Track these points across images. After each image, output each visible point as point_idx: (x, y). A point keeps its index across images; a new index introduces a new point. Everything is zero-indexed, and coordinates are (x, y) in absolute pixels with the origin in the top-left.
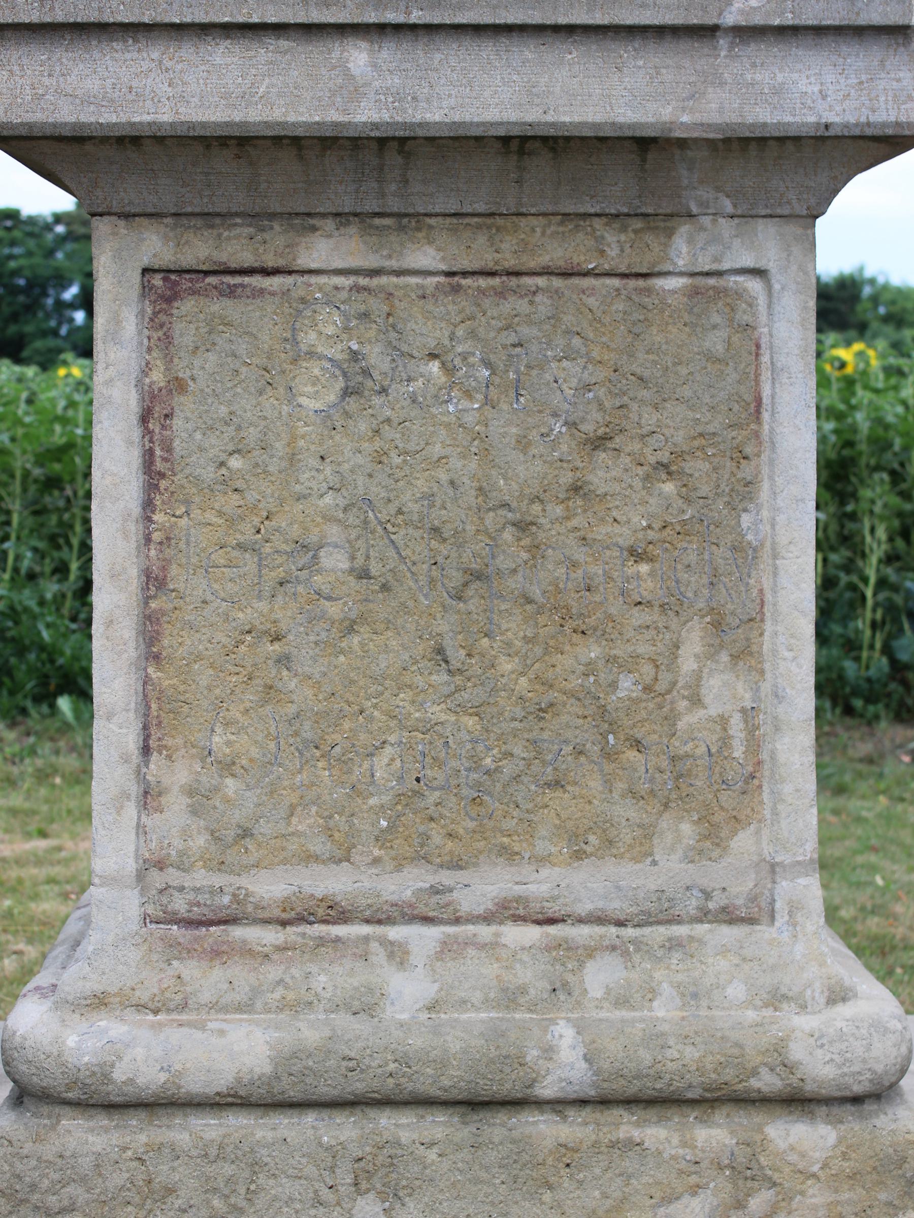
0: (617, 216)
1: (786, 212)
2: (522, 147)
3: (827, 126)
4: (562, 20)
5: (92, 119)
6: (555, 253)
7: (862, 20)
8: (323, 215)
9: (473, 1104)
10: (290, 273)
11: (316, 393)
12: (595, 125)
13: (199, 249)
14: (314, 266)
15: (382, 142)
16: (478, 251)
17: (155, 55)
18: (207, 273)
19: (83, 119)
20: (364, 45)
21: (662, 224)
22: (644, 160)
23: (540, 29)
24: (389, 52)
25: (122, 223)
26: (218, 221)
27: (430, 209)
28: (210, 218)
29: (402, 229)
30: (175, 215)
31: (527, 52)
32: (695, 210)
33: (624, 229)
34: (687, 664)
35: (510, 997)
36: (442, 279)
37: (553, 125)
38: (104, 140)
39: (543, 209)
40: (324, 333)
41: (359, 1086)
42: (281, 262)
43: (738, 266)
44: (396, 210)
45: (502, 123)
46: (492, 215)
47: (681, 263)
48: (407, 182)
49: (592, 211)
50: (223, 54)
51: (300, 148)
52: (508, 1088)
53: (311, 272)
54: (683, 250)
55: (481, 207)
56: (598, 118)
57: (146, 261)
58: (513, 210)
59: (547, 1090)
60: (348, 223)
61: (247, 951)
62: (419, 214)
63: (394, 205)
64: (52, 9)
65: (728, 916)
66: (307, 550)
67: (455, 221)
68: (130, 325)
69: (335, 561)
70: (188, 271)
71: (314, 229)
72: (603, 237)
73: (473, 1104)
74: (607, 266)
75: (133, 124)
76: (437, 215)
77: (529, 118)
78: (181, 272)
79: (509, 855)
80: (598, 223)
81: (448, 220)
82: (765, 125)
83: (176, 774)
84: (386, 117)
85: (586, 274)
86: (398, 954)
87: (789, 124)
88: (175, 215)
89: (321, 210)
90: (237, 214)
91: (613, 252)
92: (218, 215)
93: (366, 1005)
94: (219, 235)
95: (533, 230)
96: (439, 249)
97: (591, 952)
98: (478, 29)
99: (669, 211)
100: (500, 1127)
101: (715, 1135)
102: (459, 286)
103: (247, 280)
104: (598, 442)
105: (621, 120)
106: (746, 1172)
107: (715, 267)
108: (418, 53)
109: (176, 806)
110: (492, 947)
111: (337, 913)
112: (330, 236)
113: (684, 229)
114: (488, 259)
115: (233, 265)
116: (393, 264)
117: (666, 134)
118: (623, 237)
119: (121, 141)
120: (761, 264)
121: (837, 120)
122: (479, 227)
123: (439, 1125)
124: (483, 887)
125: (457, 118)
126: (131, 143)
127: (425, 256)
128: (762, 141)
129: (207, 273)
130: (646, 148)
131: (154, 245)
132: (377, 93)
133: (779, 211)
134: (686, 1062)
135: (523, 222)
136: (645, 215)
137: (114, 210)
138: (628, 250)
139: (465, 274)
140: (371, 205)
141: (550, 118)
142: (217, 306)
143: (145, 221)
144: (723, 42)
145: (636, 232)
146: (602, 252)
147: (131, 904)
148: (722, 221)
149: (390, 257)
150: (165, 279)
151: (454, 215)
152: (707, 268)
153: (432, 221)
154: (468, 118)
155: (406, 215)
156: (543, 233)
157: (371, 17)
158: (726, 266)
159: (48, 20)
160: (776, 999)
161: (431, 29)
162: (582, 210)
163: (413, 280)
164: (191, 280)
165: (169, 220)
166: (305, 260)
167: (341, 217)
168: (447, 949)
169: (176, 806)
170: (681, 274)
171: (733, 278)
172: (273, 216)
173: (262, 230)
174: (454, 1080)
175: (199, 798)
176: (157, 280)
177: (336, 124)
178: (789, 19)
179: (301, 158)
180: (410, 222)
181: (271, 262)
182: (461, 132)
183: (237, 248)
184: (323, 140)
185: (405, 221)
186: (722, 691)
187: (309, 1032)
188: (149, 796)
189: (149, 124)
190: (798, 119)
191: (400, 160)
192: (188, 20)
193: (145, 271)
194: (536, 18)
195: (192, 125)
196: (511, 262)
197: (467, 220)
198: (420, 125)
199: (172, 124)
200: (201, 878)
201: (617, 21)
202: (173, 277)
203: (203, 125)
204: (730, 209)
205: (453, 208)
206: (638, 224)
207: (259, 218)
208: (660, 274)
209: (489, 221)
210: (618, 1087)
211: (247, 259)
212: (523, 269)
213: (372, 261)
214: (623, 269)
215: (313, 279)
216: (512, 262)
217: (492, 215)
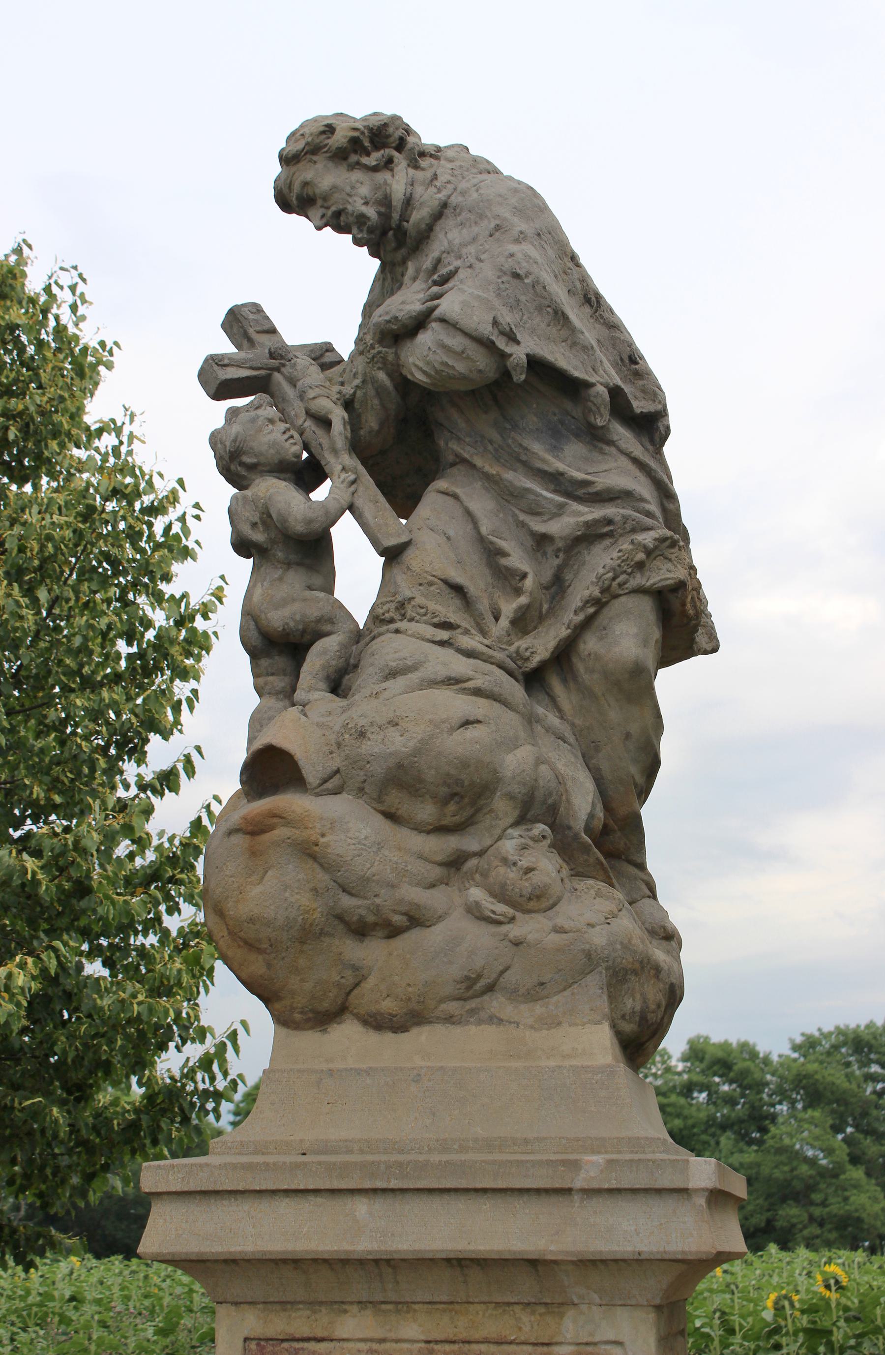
0: (529, 1304)
1: (633, 1303)
2: (460, 1264)
3: (639, 1254)
4: (479, 1186)
5: (208, 1250)
6: (491, 1327)
7: (659, 1185)
8: (351, 1303)
10: (332, 1340)
12: (498, 1252)
14: (345, 1336)
15: (376, 1261)
17: (246, 1208)
18: (283, 1340)
19: (203, 1250)
20: (365, 1200)
21: (556, 1310)
22: (537, 1270)
23: (466, 1191)
24: (379, 1205)
25: (233, 1308)
26: (289, 1306)
27: (414, 1299)
28: (284, 1304)
29: (398, 1311)
30: (264, 1303)
31: (460, 1204)
32: (576, 1301)
33: (533, 1313)
36: (423, 1345)
37: (473, 1251)
38: (216, 1261)
39: (483, 1299)
42: (325, 1334)
43: (605, 1339)
44: (393, 1299)
45: (443, 1251)
46: (452, 1303)
47: (569, 1336)
48: (398, 1282)
49: (513, 1301)
50: (285, 1207)
51: (330, 1264)
53: (343, 1340)
54: (571, 1327)
55: (445, 1298)
56: (501, 1247)
57: (246, 1333)
58: (464, 1300)
60: (366, 1308)
62: (407, 1303)
63: (393, 1297)
64: (188, 1182)
67: (430, 1306)
70: (271, 1339)
71: (345, 1311)
72: (520, 1318)
74: (523, 1338)
75: (231, 1253)
76: (418, 1303)
77: (460, 1247)
78: (267, 1340)
80: (517, 1308)
81: (426, 1306)
82: (601, 1252)
84: (376, 1247)
85: (511, 1343)
87: (616, 1252)
88: (264, 1303)
89: (349, 1299)
90: (300, 1302)
91: (526, 1328)
92: (289, 1302)
94: (290, 1316)
95: (477, 1313)
96: (420, 1326)
98: (430, 1191)
99: (560, 1301)
102: (433, 1350)
103: (305, 1345)
105: (514, 1248)
107: (590, 1339)
112: (355, 1316)
113: (571, 1313)
114: (449, 1332)
115: (297, 1336)
116: (392, 1335)
117: (542, 1257)
118: (533, 1318)
119: (226, 1261)
120: (619, 1338)
121: (645, 1249)
122: (444, 1311)
125: (417, 1248)
126: (232, 1264)
128: (603, 1261)
129: (283, 1340)
132: (371, 1231)
133: (629, 1302)
135: (471, 1308)
136: (546, 1304)
137: (229, 1299)
138: (536, 1327)
139: (437, 1342)
140: (379, 1297)
141: (472, 1247)
143: (245, 1306)
144: (576, 1197)
145: (541, 1315)
146: (520, 1328)
148: (594, 1308)
149: (391, 1330)
150: (258, 1345)
151: (430, 1303)
152: (585, 1340)
153: (416, 1307)
154: (423, 1247)
155: (400, 1303)
156: (484, 1315)
157: (368, 1185)
158: (597, 1339)
159: (186, 1189)
161: (403, 1191)
162: (506, 1300)
163: (405, 1346)
164: (273, 1345)
165: (261, 1306)
166: (340, 1333)
167: (362, 1304)
170: (570, 1344)
171: (603, 1347)
172: (321, 1303)
173: (314, 1312)
176: (253, 1345)
177: (346, 1252)
178: (614, 1184)
179: (332, 1269)
180: (403, 1307)
181: (320, 1334)
182: (420, 1256)
184: (341, 1261)
185: (400, 1306)
189: (240, 1252)
190: (621, 1248)
191: (390, 1270)
192: (264, 1188)
193: (246, 1339)
194: (463, 1184)
195: (264, 1253)
196: (463, 1335)
197: (438, 1306)
198: (395, 1252)
199: (253, 1253)
201: (511, 1186)
202: (262, 1343)
203: (270, 1252)
204: (598, 1301)
205: (429, 1298)
206: (542, 1309)
207: (314, 1305)
208: (557, 1344)
209: (451, 1307)
211: (306, 1332)
212: (472, 1339)
213: (379, 1334)
214: (533, 1340)
215: (346, 1345)
216: (465, 1335)
217: (452, 1303)
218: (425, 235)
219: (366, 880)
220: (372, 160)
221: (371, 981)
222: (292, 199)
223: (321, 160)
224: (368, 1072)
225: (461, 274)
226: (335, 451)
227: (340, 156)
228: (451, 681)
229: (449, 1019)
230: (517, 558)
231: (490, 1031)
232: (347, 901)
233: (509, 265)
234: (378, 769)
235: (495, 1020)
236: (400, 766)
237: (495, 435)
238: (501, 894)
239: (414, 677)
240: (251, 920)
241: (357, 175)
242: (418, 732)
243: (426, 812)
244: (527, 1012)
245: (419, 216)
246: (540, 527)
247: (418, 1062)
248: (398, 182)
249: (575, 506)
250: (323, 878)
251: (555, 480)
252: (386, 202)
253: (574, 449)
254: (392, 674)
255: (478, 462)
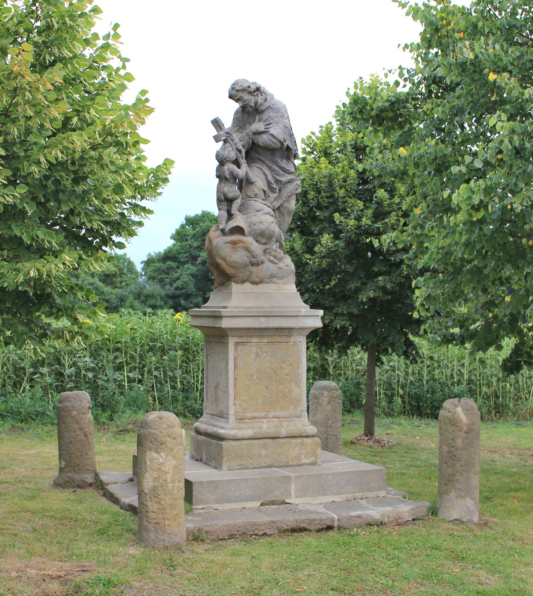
6: (279, 340)
9: (273, 438)
11: (253, 357)
13: (241, 340)
16: (271, 340)
24: (265, 318)
28: (242, 336)
31: (279, 318)
34: (293, 387)
35: (276, 426)
40: (254, 349)
41: (262, 436)
50: (248, 319)
52: (278, 436)
54: (292, 339)
59: (282, 436)
61: (246, 422)
65: (298, 417)
66: (252, 375)
68: (233, 349)
69: (255, 376)
73: (273, 438)
79: (274, 410)
83: (238, 402)
86: (263, 422)
93: (261, 428)
97: (283, 421)
100: (276, 440)
101: (299, 440)
104: (283, 362)
106: (302, 444)
108: (268, 318)
109: (238, 406)
110: (273, 421)
111: (255, 418)
123: (270, 440)
124: (271, 414)
127: (265, 340)
130: (291, 329)
131: (236, 340)
134: (296, 432)
142: (242, 347)
147: (234, 418)
160: (304, 426)
168: (268, 422)
169: (238, 406)
174: (272, 435)
175: (241, 405)
180: (263, 336)
183: (244, 340)
186: (297, 391)
187: (256, 430)
188: (235, 405)
200: (241, 414)
207: (247, 336)
210: (289, 435)
218: (263, 112)
219: (257, 255)
220: (255, 94)
221: (254, 275)
222: (231, 97)
223: (245, 93)
224: (253, 293)
225: (274, 124)
226: (242, 158)
227: (250, 93)
228: (269, 213)
229: (267, 283)
230: (275, 186)
231: (274, 285)
232: (253, 259)
233: (285, 125)
234: (258, 232)
235: (275, 283)
236: (262, 232)
237: (270, 156)
238: (275, 257)
239: (262, 212)
240: (234, 262)
241: (252, 97)
242: (266, 225)
243: (264, 241)
244: (281, 282)
245: (262, 108)
246: (279, 178)
247: (261, 291)
248: (260, 100)
249: (287, 175)
250: (249, 254)
251: (283, 169)
252: (256, 103)
253: (284, 161)
254: (258, 211)
255: (267, 162)
